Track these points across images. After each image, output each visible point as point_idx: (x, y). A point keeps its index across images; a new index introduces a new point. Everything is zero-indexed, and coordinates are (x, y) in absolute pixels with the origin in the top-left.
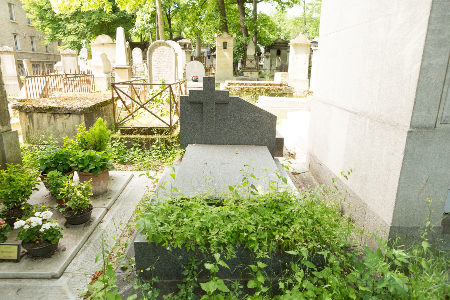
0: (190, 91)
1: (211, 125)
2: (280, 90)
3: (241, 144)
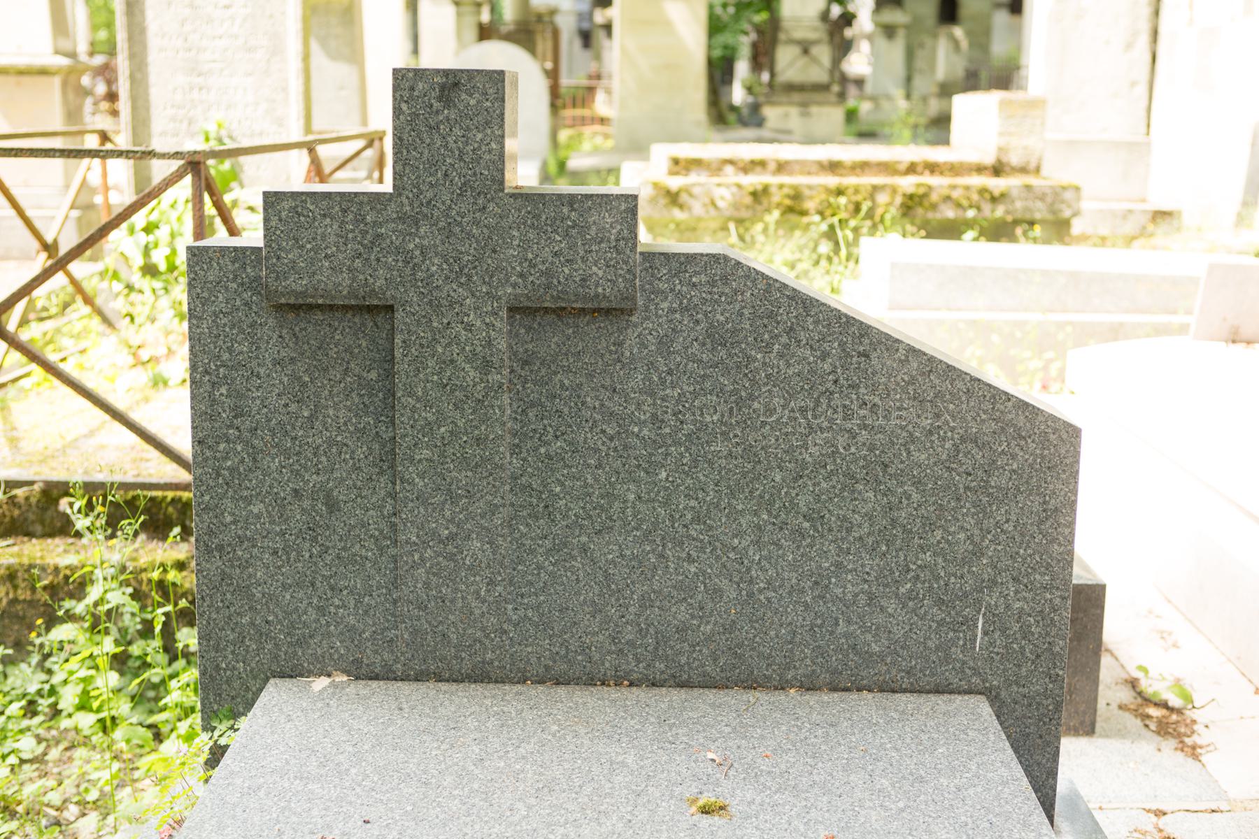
0: (272, 200)
1: (479, 507)
2: (994, 200)
3: (751, 683)
